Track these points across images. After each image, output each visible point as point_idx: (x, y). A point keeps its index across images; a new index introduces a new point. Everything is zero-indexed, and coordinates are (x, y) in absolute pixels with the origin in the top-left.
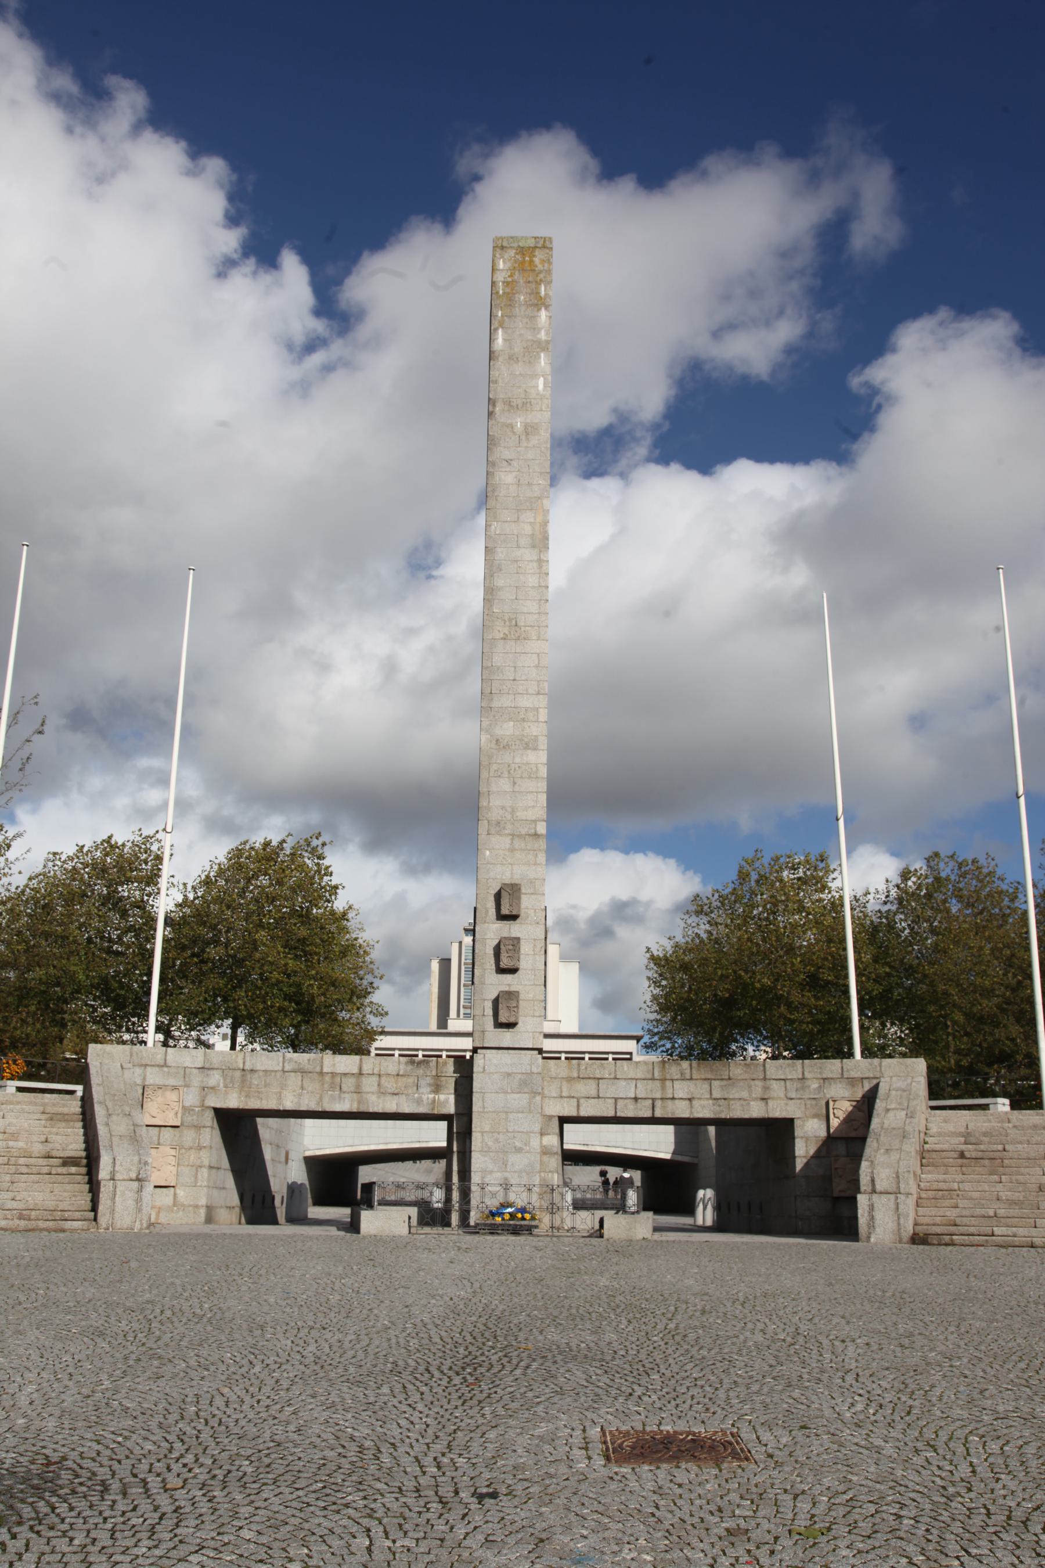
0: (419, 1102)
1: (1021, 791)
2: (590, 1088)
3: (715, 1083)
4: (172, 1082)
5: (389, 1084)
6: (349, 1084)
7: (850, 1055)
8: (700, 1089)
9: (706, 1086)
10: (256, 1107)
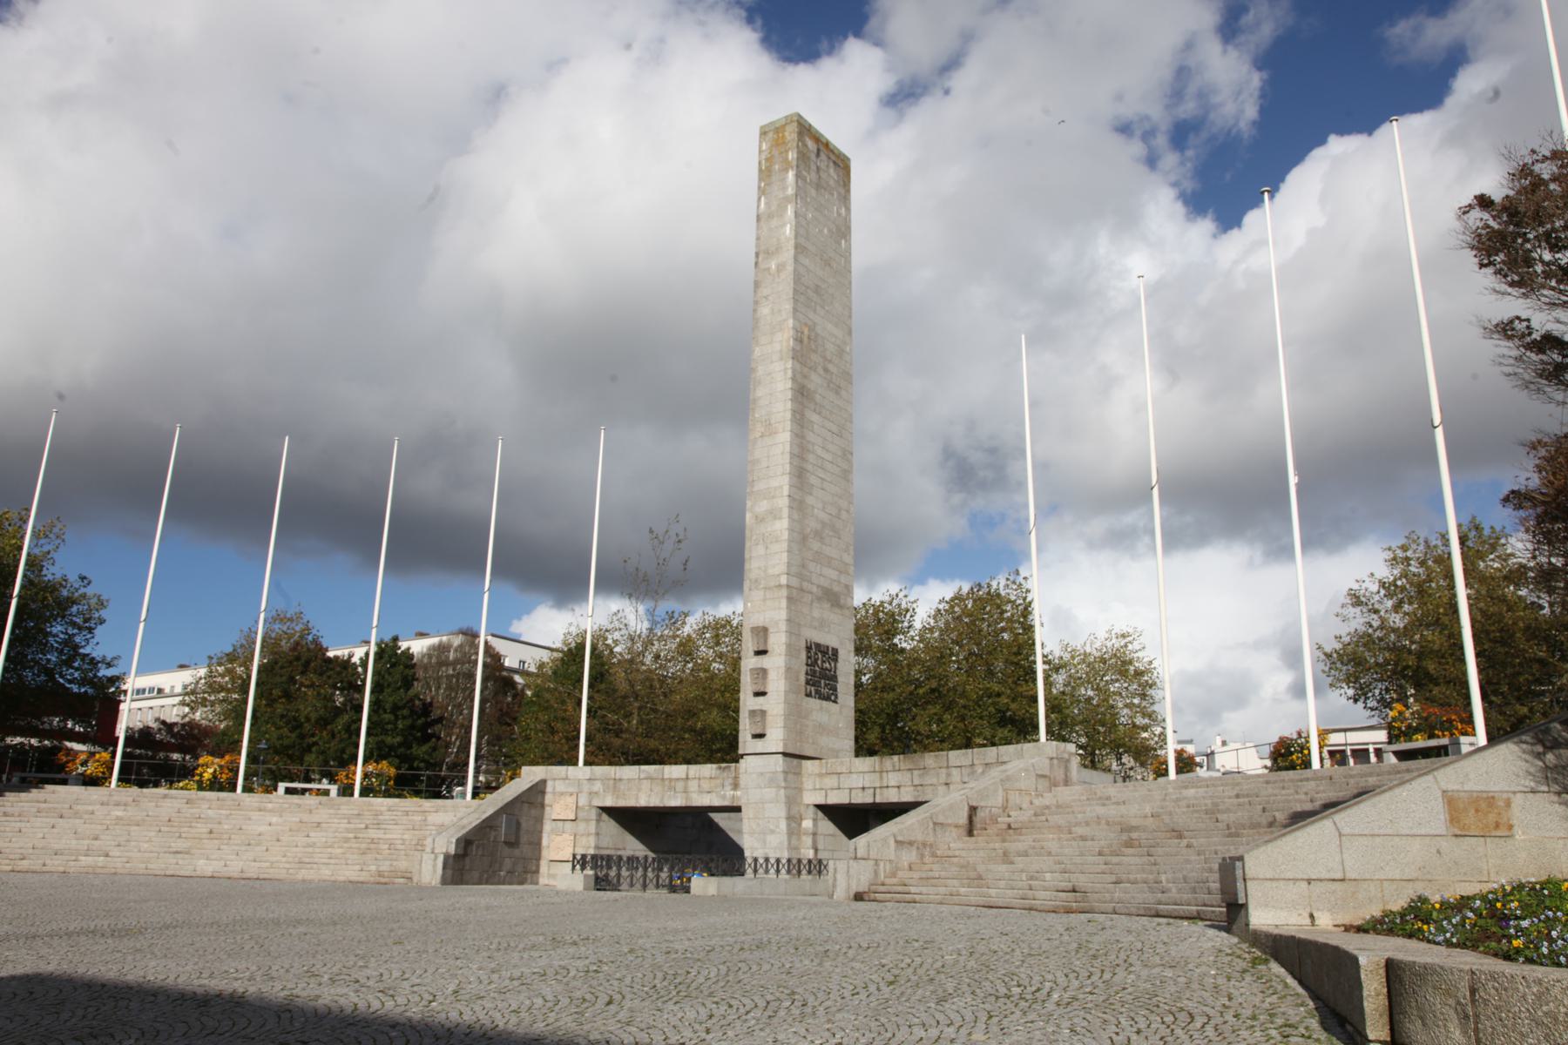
0: (724, 797)
1: (1437, 419)
2: (831, 782)
3: (916, 773)
4: (571, 790)
5: (706, 785)
6: (680, 786)
7: (352, 795)
8: (903, 778)
9: (908, 775)
10: (895, 800)
